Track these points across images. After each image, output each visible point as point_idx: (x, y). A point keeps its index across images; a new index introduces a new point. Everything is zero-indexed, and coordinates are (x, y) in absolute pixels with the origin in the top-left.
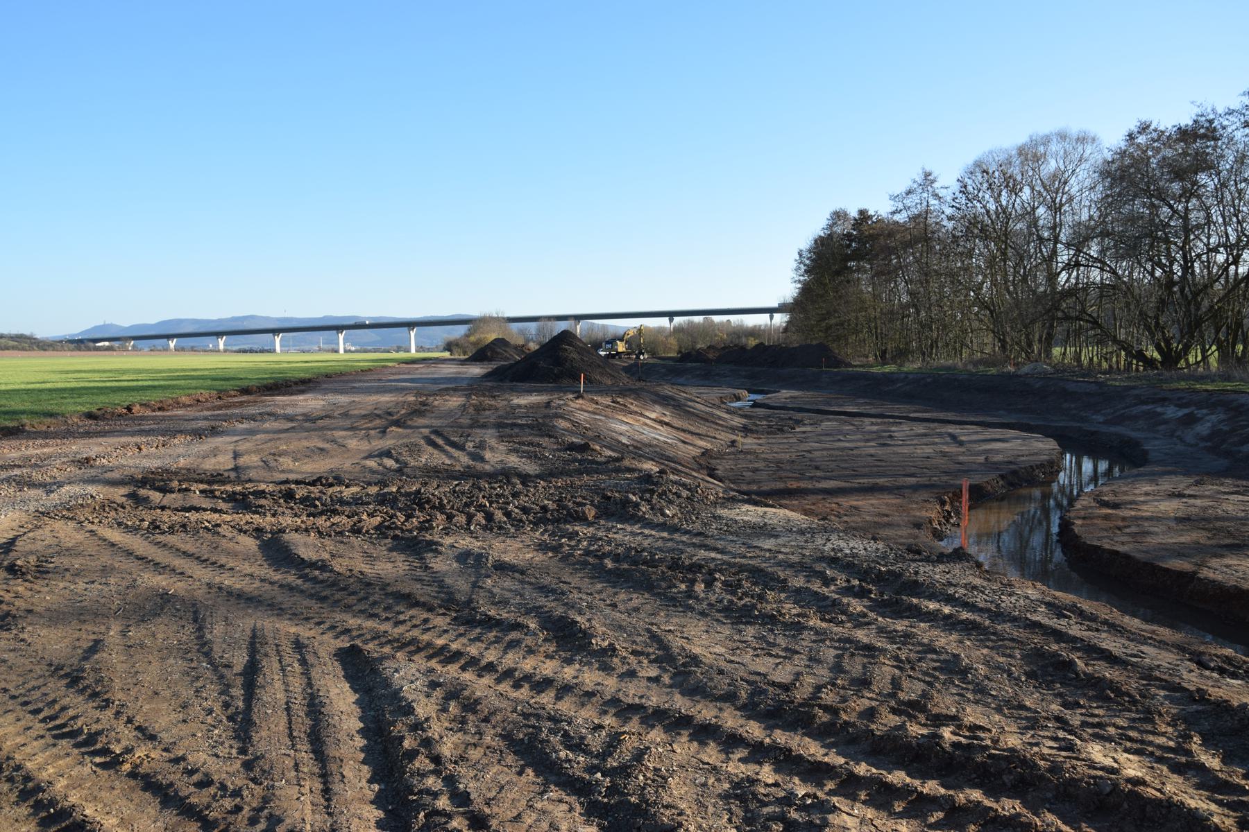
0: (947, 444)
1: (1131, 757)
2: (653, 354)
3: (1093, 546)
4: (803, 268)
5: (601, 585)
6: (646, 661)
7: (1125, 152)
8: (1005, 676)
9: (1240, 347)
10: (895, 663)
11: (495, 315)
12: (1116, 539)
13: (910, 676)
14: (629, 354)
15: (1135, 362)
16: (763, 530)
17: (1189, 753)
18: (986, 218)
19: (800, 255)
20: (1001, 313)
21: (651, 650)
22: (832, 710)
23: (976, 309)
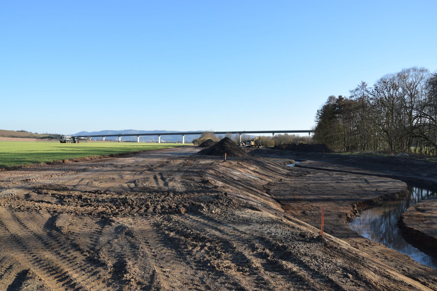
0: (362, 182)
2: (266, 147)
11: (210, 131)
12: (420, 225)
14: (255, 146)
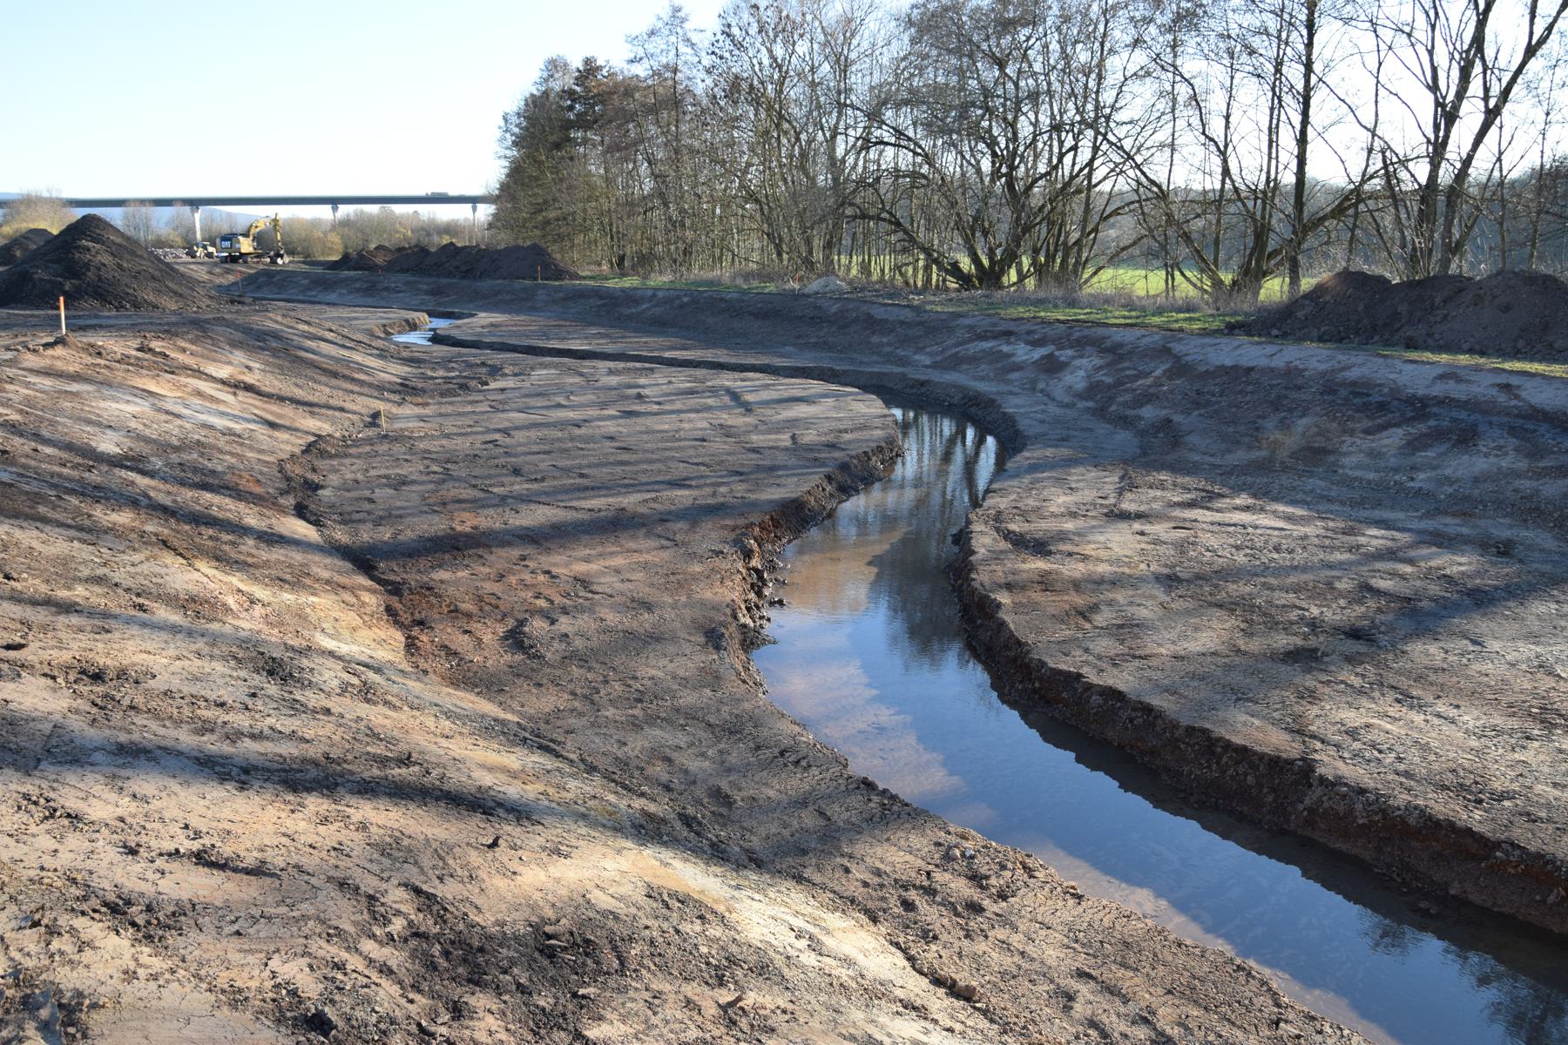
0: (724, 408)
3: (1060, 672)
4: (510, 139)
11: (46, 194)
14: (259, 256)
19: (506, 120)
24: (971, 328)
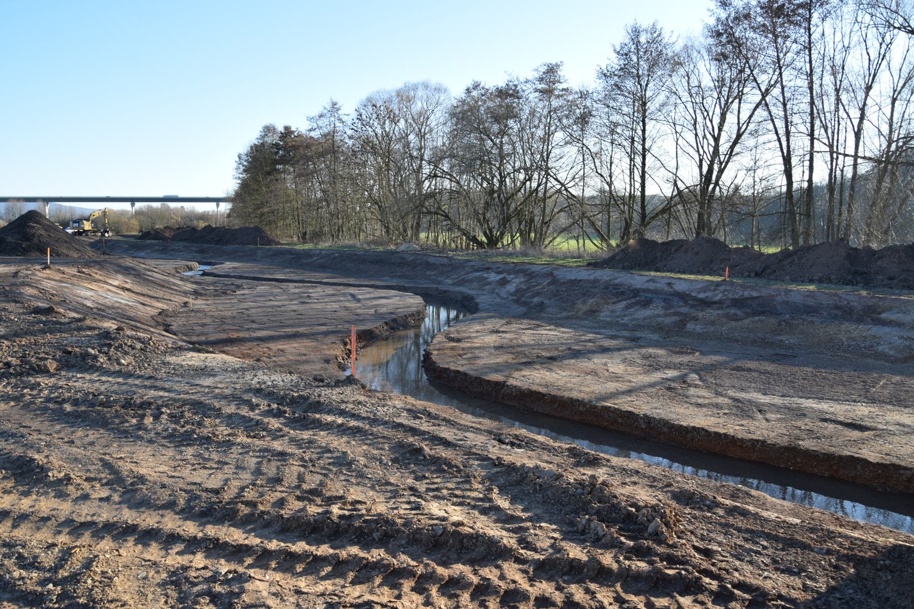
0: (348, 301)
1: (456, 508)
2: (117, 232)
4: (242, 168)
5: (60, 426)
6: (98, 485)
7: (465, 100)
8: (378, 463)
9: (533, 235)
10: (301, 463)
12: (458, 363)
13: (311, 472)
14: (94, 232)
15: (471, 243)
16: (204, 371)
17: (490, 500)
18: (375, 139)
19: (240, 158)
20: (386, 207)
21: (103, 476)
22: (252, 504)
23: (369, 204)
24: (473, 266)
